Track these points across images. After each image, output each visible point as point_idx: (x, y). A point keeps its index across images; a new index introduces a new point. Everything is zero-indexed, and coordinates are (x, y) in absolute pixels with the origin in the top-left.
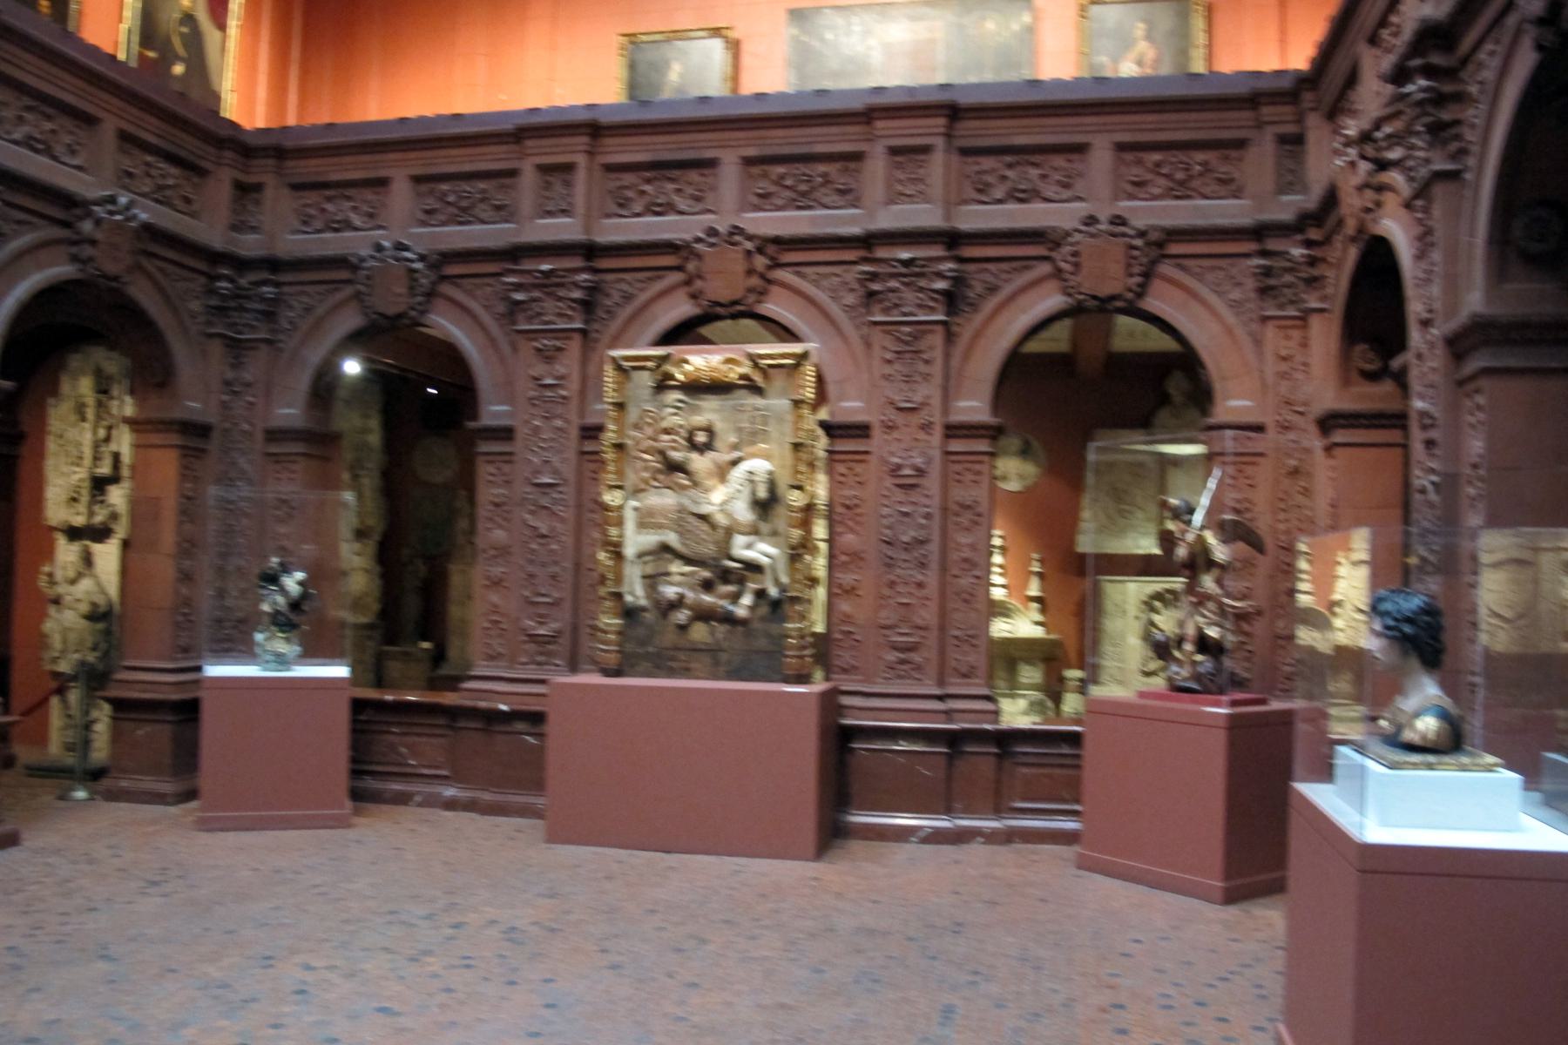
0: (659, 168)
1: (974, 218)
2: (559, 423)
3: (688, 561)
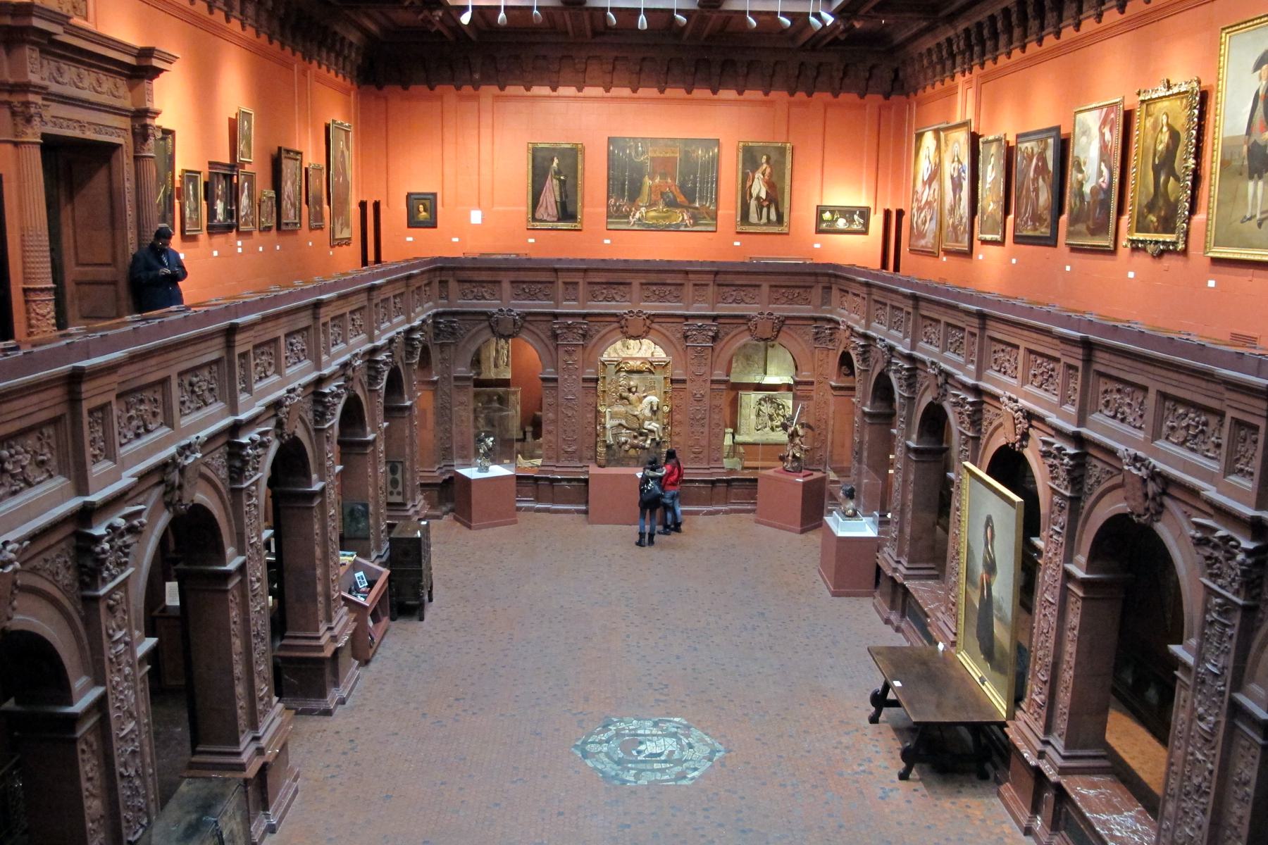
3: (628, 429)
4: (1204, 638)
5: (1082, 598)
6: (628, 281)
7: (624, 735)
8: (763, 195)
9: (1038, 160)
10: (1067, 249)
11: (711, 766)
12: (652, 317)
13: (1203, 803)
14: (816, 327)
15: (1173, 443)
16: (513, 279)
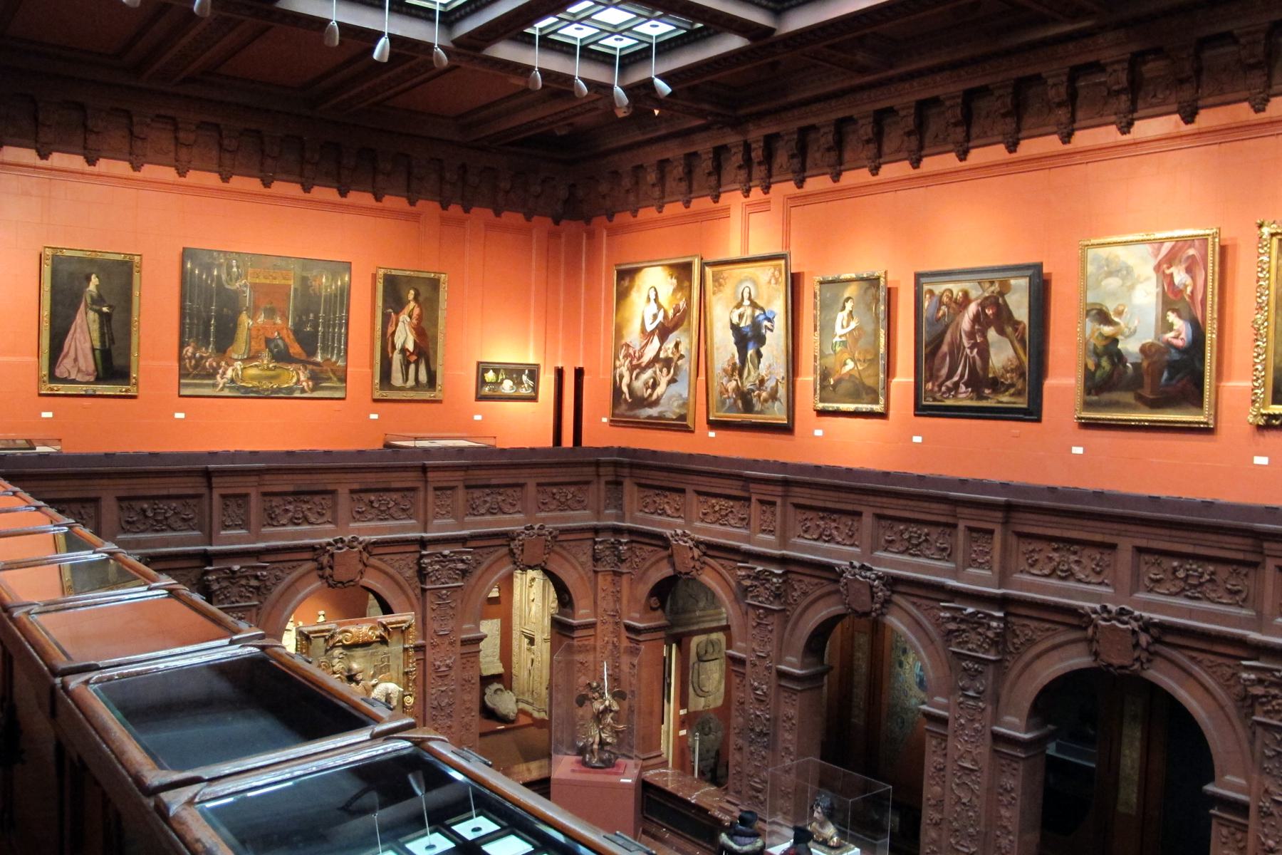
2: (977, 725)
6: (330, 487)
8: (410, 346)
12: (369, 547)
16: (122, 494)
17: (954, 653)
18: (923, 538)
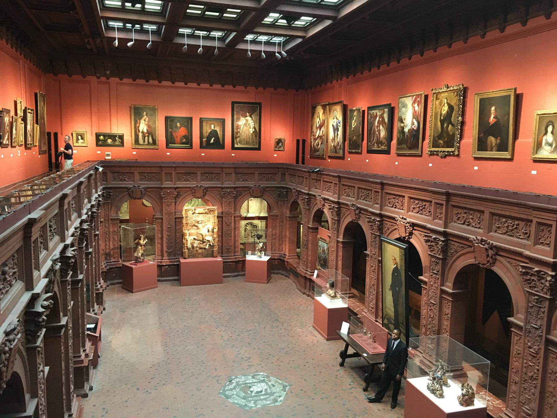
0: (186, 174)
1: (240, 184)
2: (171, 217)
3: (198, 240)
4: (528, 313)
5: (451, 301)
6: (195, 172)
7: (241, 384)
8: (145, 131)
9: (380, 118)
10: (396, 155)
11: (287, 394)
13: (535, 384)
14: (279, 191)
15: (500, 233)
17: (528, 292)
18: (515, 226)
